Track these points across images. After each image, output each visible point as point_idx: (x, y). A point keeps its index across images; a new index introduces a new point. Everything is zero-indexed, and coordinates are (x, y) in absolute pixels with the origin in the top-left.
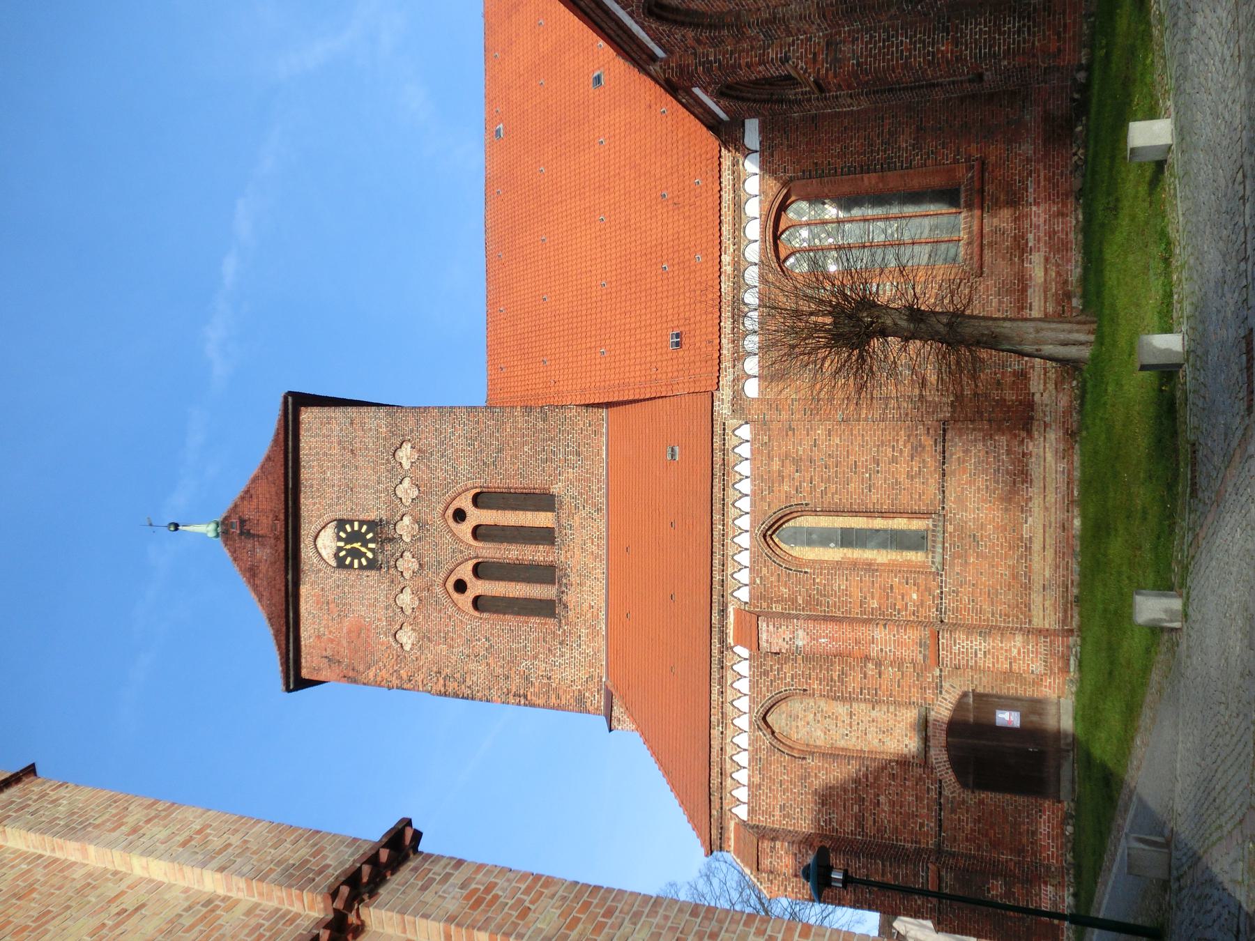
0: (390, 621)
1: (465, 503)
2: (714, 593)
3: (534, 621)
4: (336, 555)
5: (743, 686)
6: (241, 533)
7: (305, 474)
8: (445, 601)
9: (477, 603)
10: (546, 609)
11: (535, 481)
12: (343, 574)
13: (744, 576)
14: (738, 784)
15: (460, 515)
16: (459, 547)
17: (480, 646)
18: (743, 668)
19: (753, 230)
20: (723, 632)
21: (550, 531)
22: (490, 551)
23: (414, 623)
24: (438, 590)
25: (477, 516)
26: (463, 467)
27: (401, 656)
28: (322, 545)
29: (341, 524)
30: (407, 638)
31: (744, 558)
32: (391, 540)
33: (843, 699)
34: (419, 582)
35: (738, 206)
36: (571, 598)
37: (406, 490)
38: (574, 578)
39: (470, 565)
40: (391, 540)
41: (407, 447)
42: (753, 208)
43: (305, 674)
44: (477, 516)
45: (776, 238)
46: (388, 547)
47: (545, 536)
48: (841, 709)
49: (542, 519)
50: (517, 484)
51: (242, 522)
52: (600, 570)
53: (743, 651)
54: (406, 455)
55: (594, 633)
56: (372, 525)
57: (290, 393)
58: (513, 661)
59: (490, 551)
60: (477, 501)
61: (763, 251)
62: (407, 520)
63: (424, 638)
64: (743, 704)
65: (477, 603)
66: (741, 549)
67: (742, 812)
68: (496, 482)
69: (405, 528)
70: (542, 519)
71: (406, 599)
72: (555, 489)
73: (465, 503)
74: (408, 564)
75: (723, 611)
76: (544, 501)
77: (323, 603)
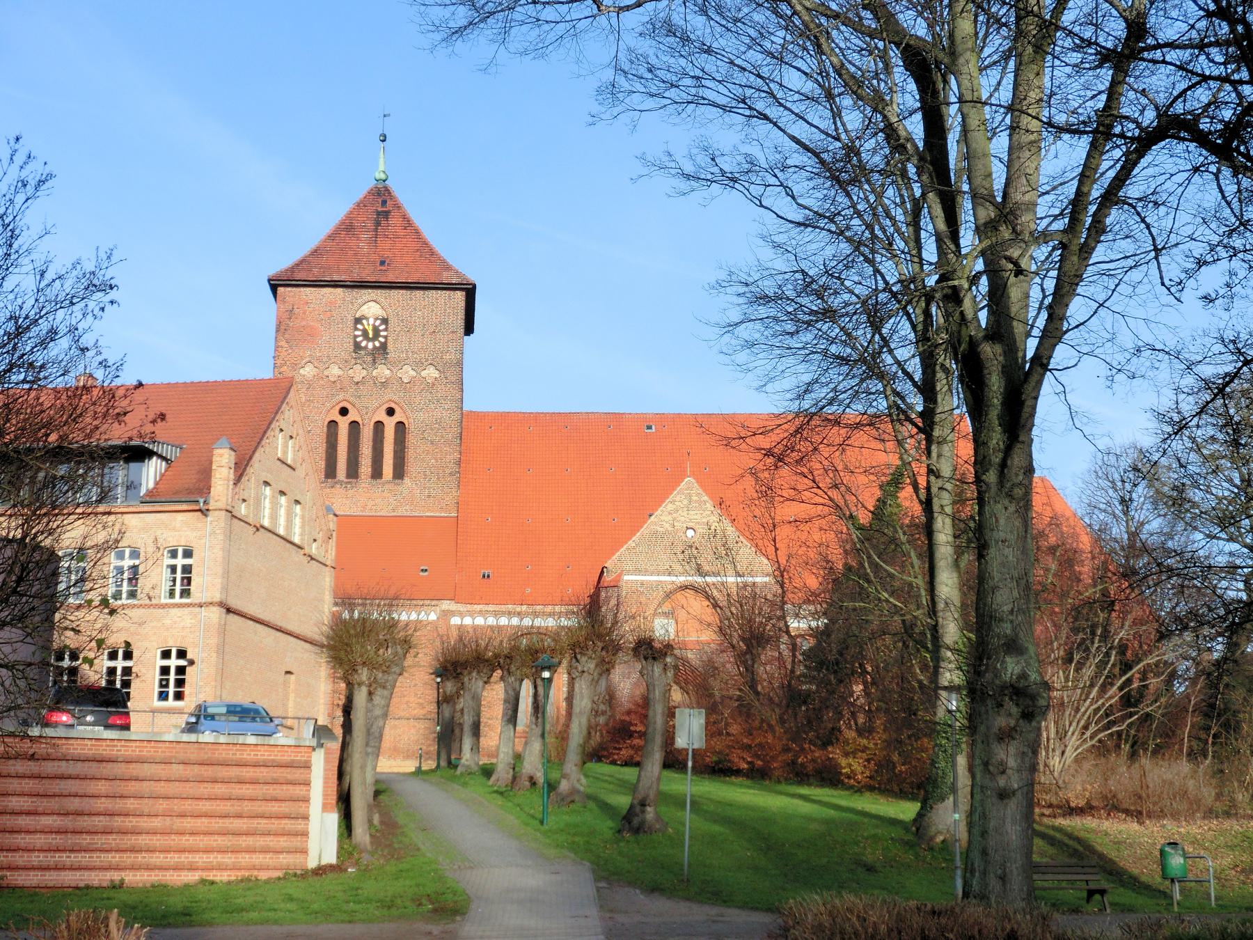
0: (319, 359)
3: (322, 464)
10: (330, 472)
11: (412, 466)
12: (350, 323)
15: (391, 412)
23: (319, 377)
24: (341, 397)
28: (371, 307)
29: (385, 321)
37: (408, 373)
38: (351, 492)
41: (436, 374)
44: (390, 423)
47: (377, 473)
54: (431, 373)
57: (474, 286)
62: (387, 372)
69: (383, 371)
71: (335, 371)
72: (406, 480)
74: (359, 373)
76: (399, 473)
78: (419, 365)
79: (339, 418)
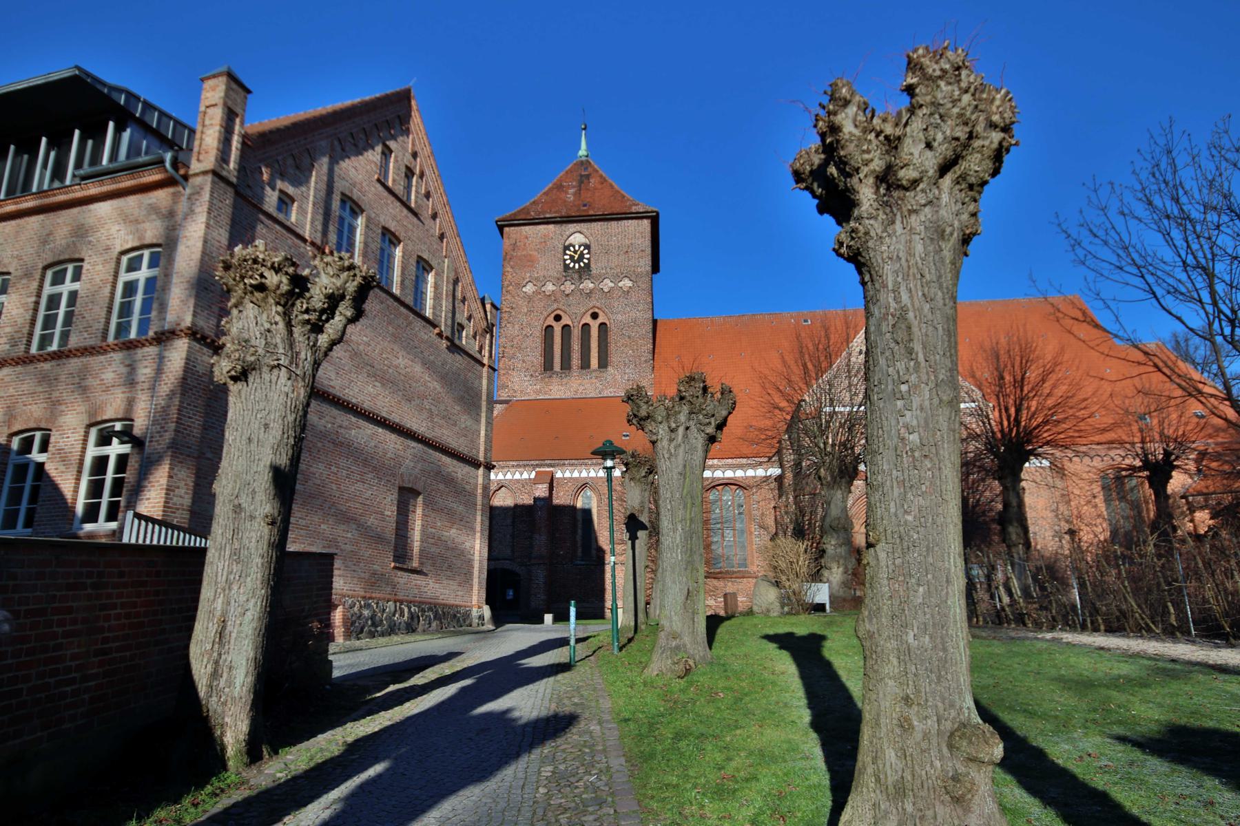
0: (537, 279)
1: (600, 320)
2: (562, 459)
3: (541, 359)
4: (571, 245)
5: (517, 476)
6: (581, 176)
7: (614, 223)
8: (549, 310)
9: (549, 328)
10: (548, 366)
11: (614, 358)
12: (561, 250)
13: (568, 475)
14: (572, 473)
15: (595, 316)
16: (575, 316)
17: (527, 331)
18: (525, 476)
19: (729, 474)
20: (541, 466)
21: (589, 366)
22: (576, 333)
23: (536, 293)
24: (555, 306)
25: (594, 326)
26: (619, 317)
27: (520, 286)
28: (577, 237)
29: (587, 247)
30: (529, 289)
31: (576, 474)
32: (580, 278)
33: (513, 522)
34: (558, 295)
35: (741, 467)
36: (555, 379)
37: (608, 284)
38: (565, 380)
39: (569, 323)
40: (580, 278)
41: (630, 284)
42: (740, 473)
43: (506, 229)
44: (594, 326)
45: (726, 484)
46: (576, 276)
47: (585, 365)
48: (509, 521)
49: (594, 362)
50: (612, 348)
51: (588, 177)
52: (569, 395)
53: (533, 475)
54: (627, 283)
55: (539, 392)
56: (588, 266)
57: (658, 213)
58: (519, 348)
59: (576, 333)
60: (603, 325)
61: (719, 479)
62: (591, 285)
63: (529, 298)
64: (509, 476)
65: (549, 328)
66: (572, 473)
67: (559, 475)
68: (613, 337)
69: (588, 285)
70: (594, 362)
71: (550, 287)
72: (609, 368)
73: (600, 320)
74: (569, 287)
75: (550, 465)
76: (603, 364)
77: (545, 239)
78: (617, 278)
79: (554, 324)
